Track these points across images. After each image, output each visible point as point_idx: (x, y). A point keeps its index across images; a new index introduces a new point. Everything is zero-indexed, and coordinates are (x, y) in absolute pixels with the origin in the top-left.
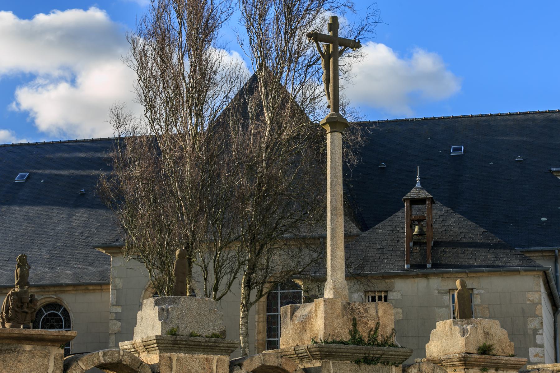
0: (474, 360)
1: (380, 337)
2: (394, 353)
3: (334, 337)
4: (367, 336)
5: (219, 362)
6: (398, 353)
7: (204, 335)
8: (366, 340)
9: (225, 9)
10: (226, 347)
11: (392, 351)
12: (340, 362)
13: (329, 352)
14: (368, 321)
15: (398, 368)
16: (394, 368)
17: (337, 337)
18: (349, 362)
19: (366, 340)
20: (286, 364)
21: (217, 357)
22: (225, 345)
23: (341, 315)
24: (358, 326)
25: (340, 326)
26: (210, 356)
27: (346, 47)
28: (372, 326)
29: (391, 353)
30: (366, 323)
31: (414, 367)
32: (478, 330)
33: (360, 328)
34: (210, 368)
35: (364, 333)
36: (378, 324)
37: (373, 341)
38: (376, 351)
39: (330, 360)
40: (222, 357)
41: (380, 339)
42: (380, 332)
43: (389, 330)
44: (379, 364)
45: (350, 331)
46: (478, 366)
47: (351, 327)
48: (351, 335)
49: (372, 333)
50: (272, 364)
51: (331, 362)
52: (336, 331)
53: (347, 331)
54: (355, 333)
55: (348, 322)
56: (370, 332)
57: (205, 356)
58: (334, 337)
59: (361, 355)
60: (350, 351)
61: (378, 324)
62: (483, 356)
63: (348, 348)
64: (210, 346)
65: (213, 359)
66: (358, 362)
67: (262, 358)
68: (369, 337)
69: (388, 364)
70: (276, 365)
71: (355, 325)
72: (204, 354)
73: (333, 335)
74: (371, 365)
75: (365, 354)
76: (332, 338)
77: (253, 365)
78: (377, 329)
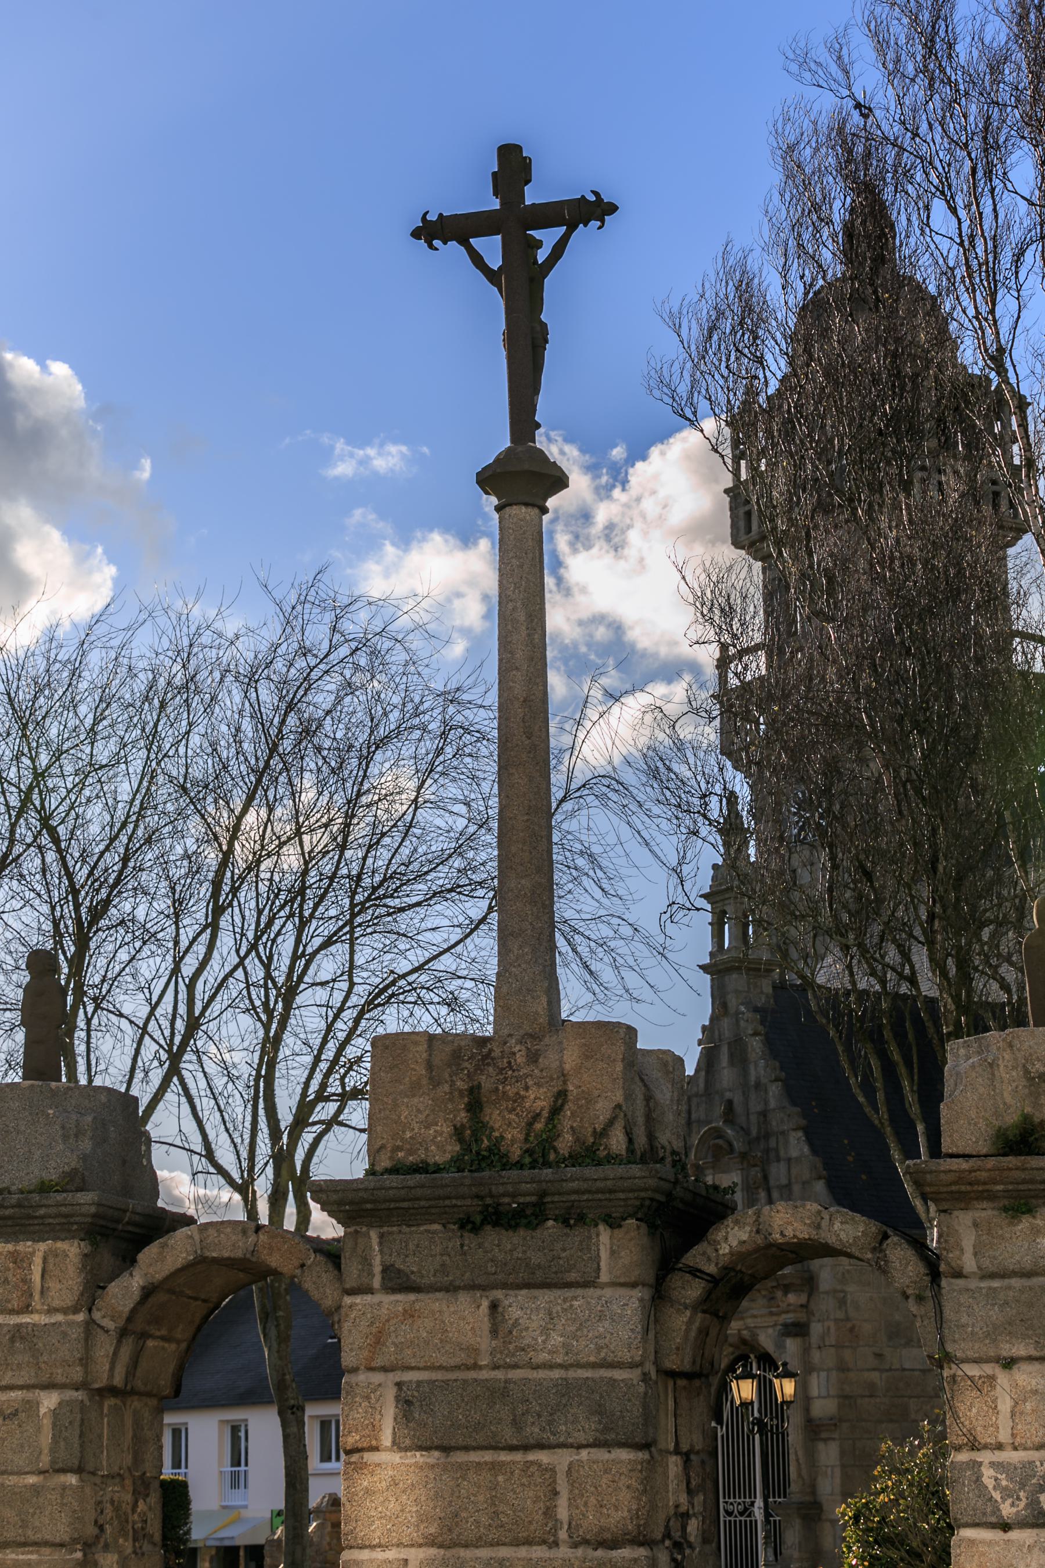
0: (950, 1177)
1: (569, 1137)
2: (585, 1186)
3: (400, 1154)
4: (521, 1137)
5: (51, 1260)
6: (600, 1185)
7: (14, 1188)
8: (516, 1153)
9: (963, 138)
10: (56, 1216)
11: (572, 1179)
12: (405, 1229)
13: (351, 1203)
14: (527, 1088)
15: (618, 1233)
16: (604, 1236)
17: (410, 1152)
18: (436, 1227)
19: (516, 1153)
20: (271, 1248)
21: (42, 1247)
22: (52, 1211)
23: (424, 1081)
24: (487, 1110)
25: (422, 1117)
26: (25, 1246)
27: (572, 228)
28: (540, 1104)
29: (575, 1185)
30: (518, 1099)
31: (737, 1222)
32: (1002, 1072)
33: (495, 1117)
34: (24, 1281)
35: (508, 1129)
36: (562, 1095)
37: (540, 1153)
38: (518, 1186)
39: (370, 1226)
40: (59, 1244)
41: (565, 1143)
42: (567, 1121)
43: (602, 1110)
44: (550, 1223)
45: (458, 1132)
46: (990, 1196)
47: (463, 1116)
48: (461, 1140)
49: (539, 1126)
50: (226, 1255)
51: (374, 1235)
52: (408, 1135)
53: (447, 1129)
54: (474, 1133)
55: (451, 1100)
56: (530, 1124)
57: (10, 1247)
58: (400, 1154)
59: (468, 1202)
60: (419, 1192)
61: (562, 1095)
62: (1012, 1161)
63: (411, 1183)
64: (9, 1218)
65: (33, 1254)
66: (468, 1224)
67: (197, 1237)
68: (526, 1140)
69: (581, 1219)
70: (239, 1254)
71: (475, 1104)
72: (7, 1242)
73: (399, 1149)
74: (522, 1232)
75: (480, 1197)
76: (391, 1158)
77: (169, 1260)
78: (556, 1111)
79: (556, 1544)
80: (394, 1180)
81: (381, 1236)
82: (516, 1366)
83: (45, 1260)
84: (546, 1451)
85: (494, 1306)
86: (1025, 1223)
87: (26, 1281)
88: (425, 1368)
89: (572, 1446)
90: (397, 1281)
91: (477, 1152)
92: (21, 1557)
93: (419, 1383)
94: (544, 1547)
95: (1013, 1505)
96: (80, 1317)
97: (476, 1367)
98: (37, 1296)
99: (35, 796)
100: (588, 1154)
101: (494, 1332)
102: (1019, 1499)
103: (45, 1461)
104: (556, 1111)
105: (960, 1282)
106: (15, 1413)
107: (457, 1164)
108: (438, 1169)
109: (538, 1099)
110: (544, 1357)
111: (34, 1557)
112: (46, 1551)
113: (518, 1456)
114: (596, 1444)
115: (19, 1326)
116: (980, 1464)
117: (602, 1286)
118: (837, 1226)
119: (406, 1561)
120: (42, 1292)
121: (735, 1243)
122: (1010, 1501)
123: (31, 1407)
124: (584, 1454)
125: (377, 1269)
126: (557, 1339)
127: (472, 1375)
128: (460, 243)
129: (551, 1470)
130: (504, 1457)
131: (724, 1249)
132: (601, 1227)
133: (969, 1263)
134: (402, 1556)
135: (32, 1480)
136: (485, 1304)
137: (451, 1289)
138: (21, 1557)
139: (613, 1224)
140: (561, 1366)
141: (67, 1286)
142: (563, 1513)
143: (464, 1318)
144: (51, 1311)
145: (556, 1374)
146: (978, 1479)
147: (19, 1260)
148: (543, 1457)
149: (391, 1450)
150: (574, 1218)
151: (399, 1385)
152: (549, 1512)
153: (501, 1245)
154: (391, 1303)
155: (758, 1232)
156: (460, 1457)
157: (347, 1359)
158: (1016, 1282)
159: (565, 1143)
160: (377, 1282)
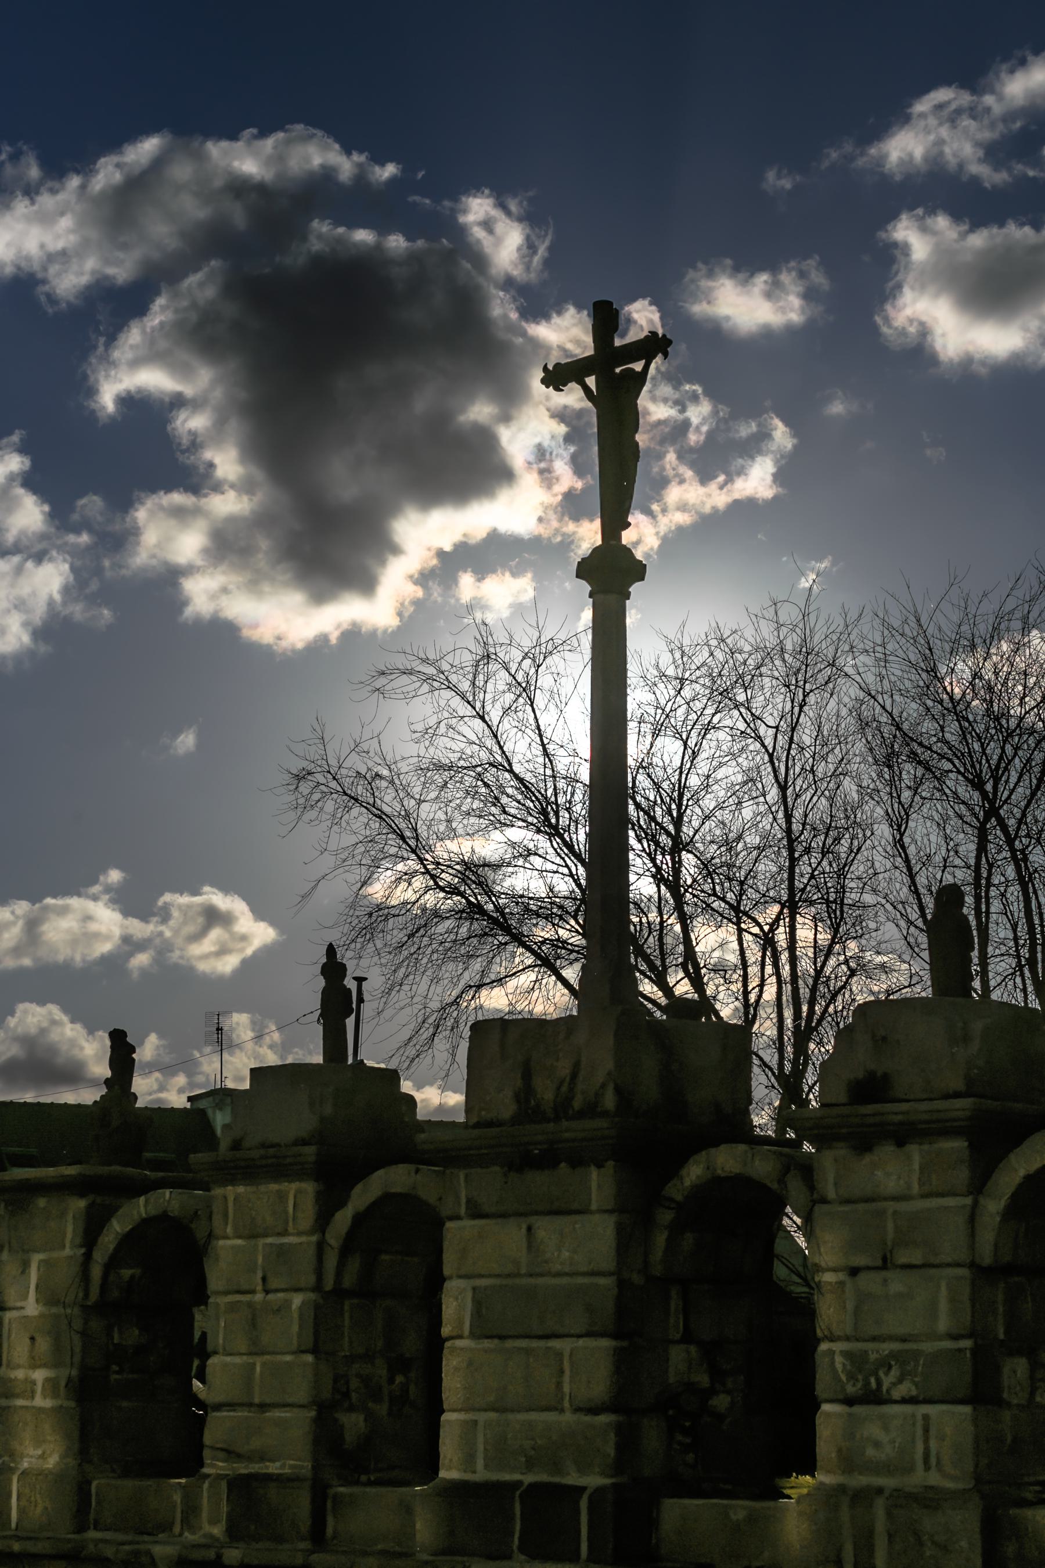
16: (594, 1174)
26: (284, 1186)
37: (562, 1109)
41: (577, 1104)
45: (517, 1097)
56: (558, 1088)
58: (483, 1113)
71: (527, 1075)
78: (574, 1076)
79: (562, 1411)
80: (476, 1132)
81: (466, 1176)
82: (542, 1275)
83: (295, 1197)
84: (559, 1340)
85: (529, 1229)
86: (868, 1158)
87: (286, 1212)
88: (490, 1276)
89: (572, 1336)
90: (476, 1213)
91: (528, 1109)
92: (283, 1415)
93: (486, 1288)
94: (557, 1413)
95: (854, 1385)
96: (314, 1238)
97: (518, 1275)
98: (291, 1224)
99: (1035, 781)
100: (592, 1110)
101: (530, 1247)
102: (857, 1380)
103: (294, 1346)
104: (574, 1076)
105: (825, 1207)
106: (278, 1310)
107: (516, 1120)
108: (499, 1124)
109: (564, 1068)
110: (558, 1267)
111: (288, 1415)
112: (295, 1410)
113: (541, 1343)
114: (588, 1334)
115: (282, 1244)
116: (834, 1352)
117: (591, 1212)
118: (757, 1163)
119: (476, 1422)
120: (294, 1220)
121: (694, 1178)
122: (851, 1383)
123: (288, 1303)
124: (581, 1342)
125: (464, 1200)
126: (566, 1254)
127: (517, 1281)
128: (578, 383)
129: (559, 1355)
130: (535, 1344)
131: (687, 1183)
132: (593, 1168)
133: (831, 1194)
134: (474, 1418)
135: (288, 1358)
136: (524, 1227)
137: (503, 1215)
138: (283, 1415)
139: (600, 1166)
140: (567, 1274)
141: (307, 1216)
142: (566, 1389)
143: (510, 1237)
144: (299, 1234)
145: (565, 1280)
146: (833, 1362)
147: (282, 1197)
148: (555, 1344)
149: (468, 1337)
150: (577, 1161)
151: (474, 1289)
152: (559, 1385)
153: (538, 1181)
154: (469, 1225)
155: (708, 1168)
156: (510, 1344)
157: (446, 1271)
158: (861, 1207)
159: (577, 1104)
160: (463, 1211)
